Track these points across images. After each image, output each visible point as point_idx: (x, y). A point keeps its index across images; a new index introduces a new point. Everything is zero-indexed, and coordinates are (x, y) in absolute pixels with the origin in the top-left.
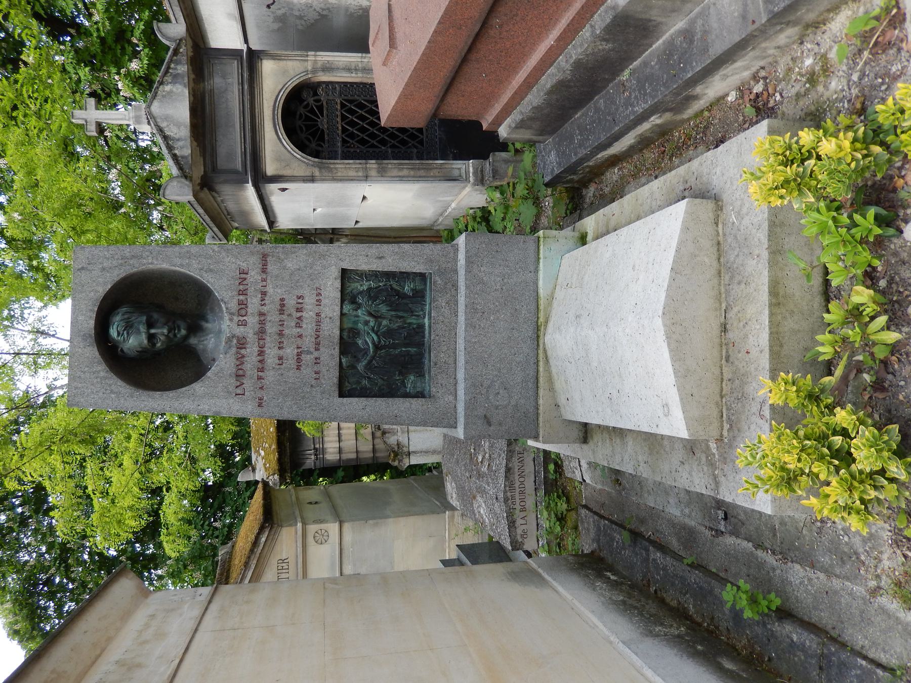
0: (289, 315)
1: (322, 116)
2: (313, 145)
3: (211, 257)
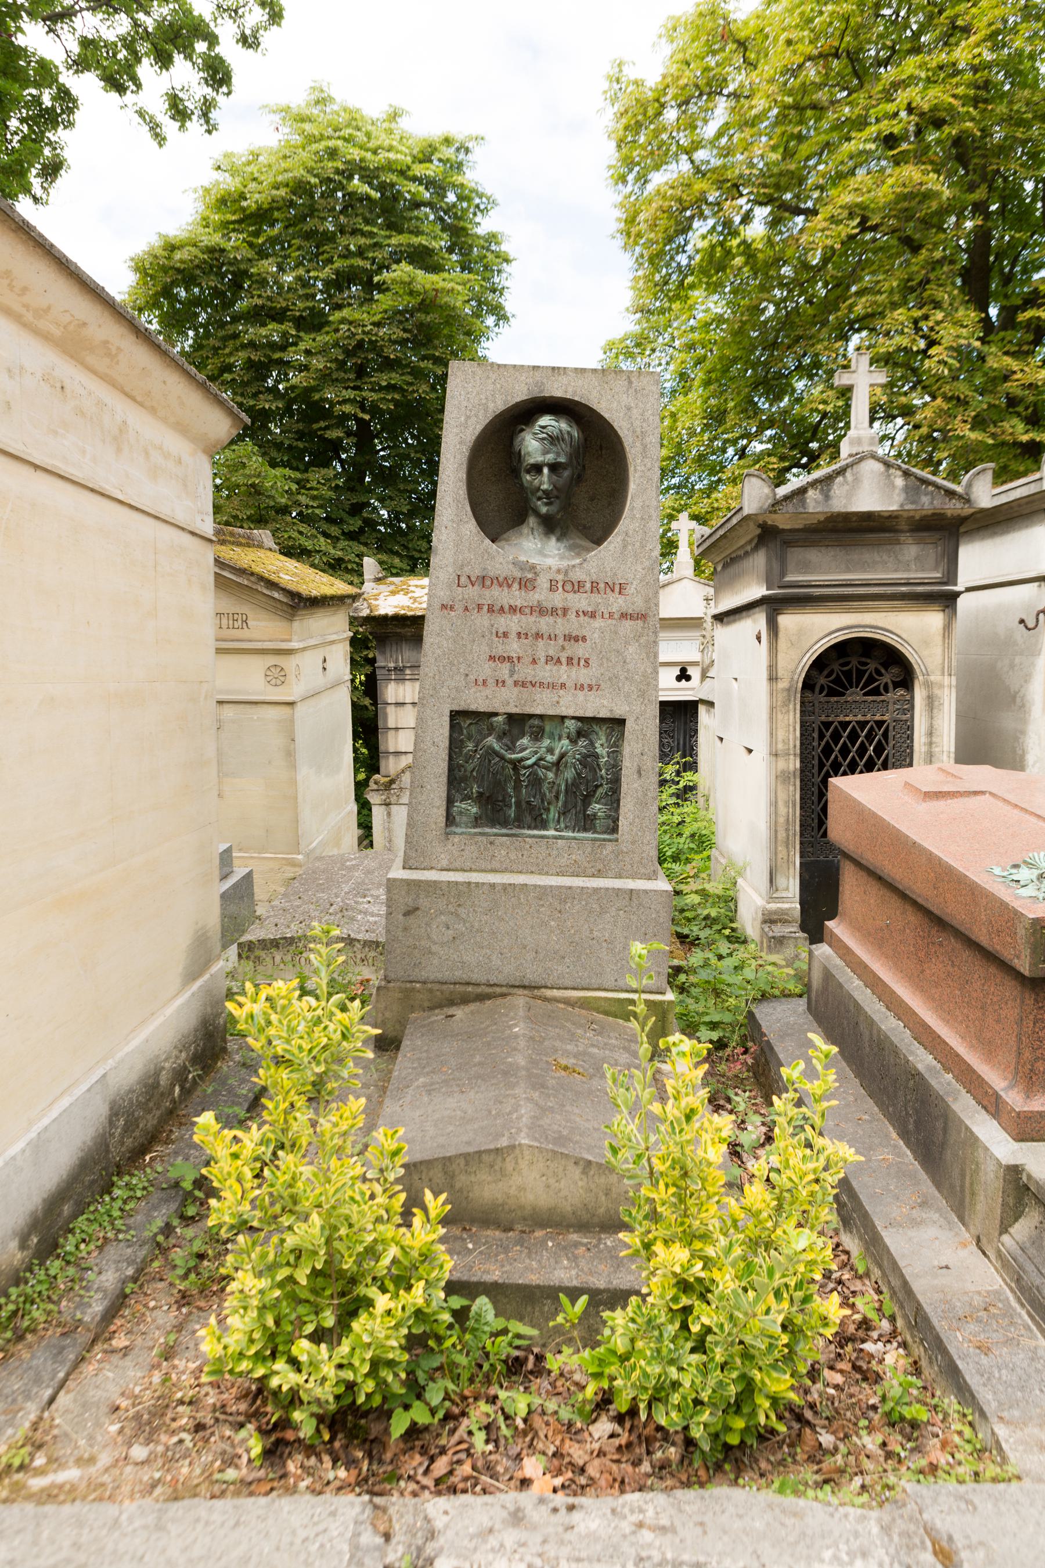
0: (563, 648)
1: (865, 694)
2: (822, 681)
3: (643, 547)
